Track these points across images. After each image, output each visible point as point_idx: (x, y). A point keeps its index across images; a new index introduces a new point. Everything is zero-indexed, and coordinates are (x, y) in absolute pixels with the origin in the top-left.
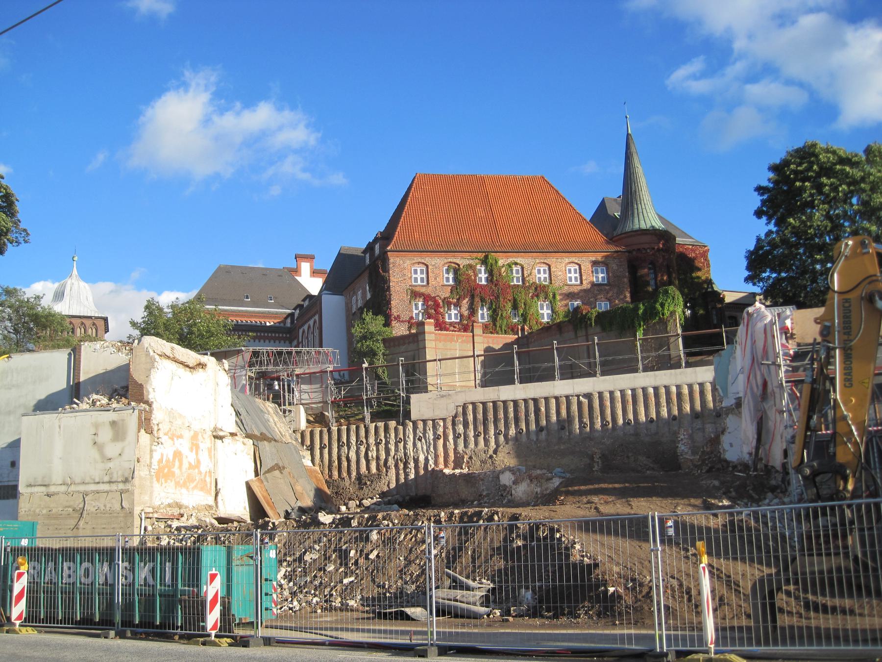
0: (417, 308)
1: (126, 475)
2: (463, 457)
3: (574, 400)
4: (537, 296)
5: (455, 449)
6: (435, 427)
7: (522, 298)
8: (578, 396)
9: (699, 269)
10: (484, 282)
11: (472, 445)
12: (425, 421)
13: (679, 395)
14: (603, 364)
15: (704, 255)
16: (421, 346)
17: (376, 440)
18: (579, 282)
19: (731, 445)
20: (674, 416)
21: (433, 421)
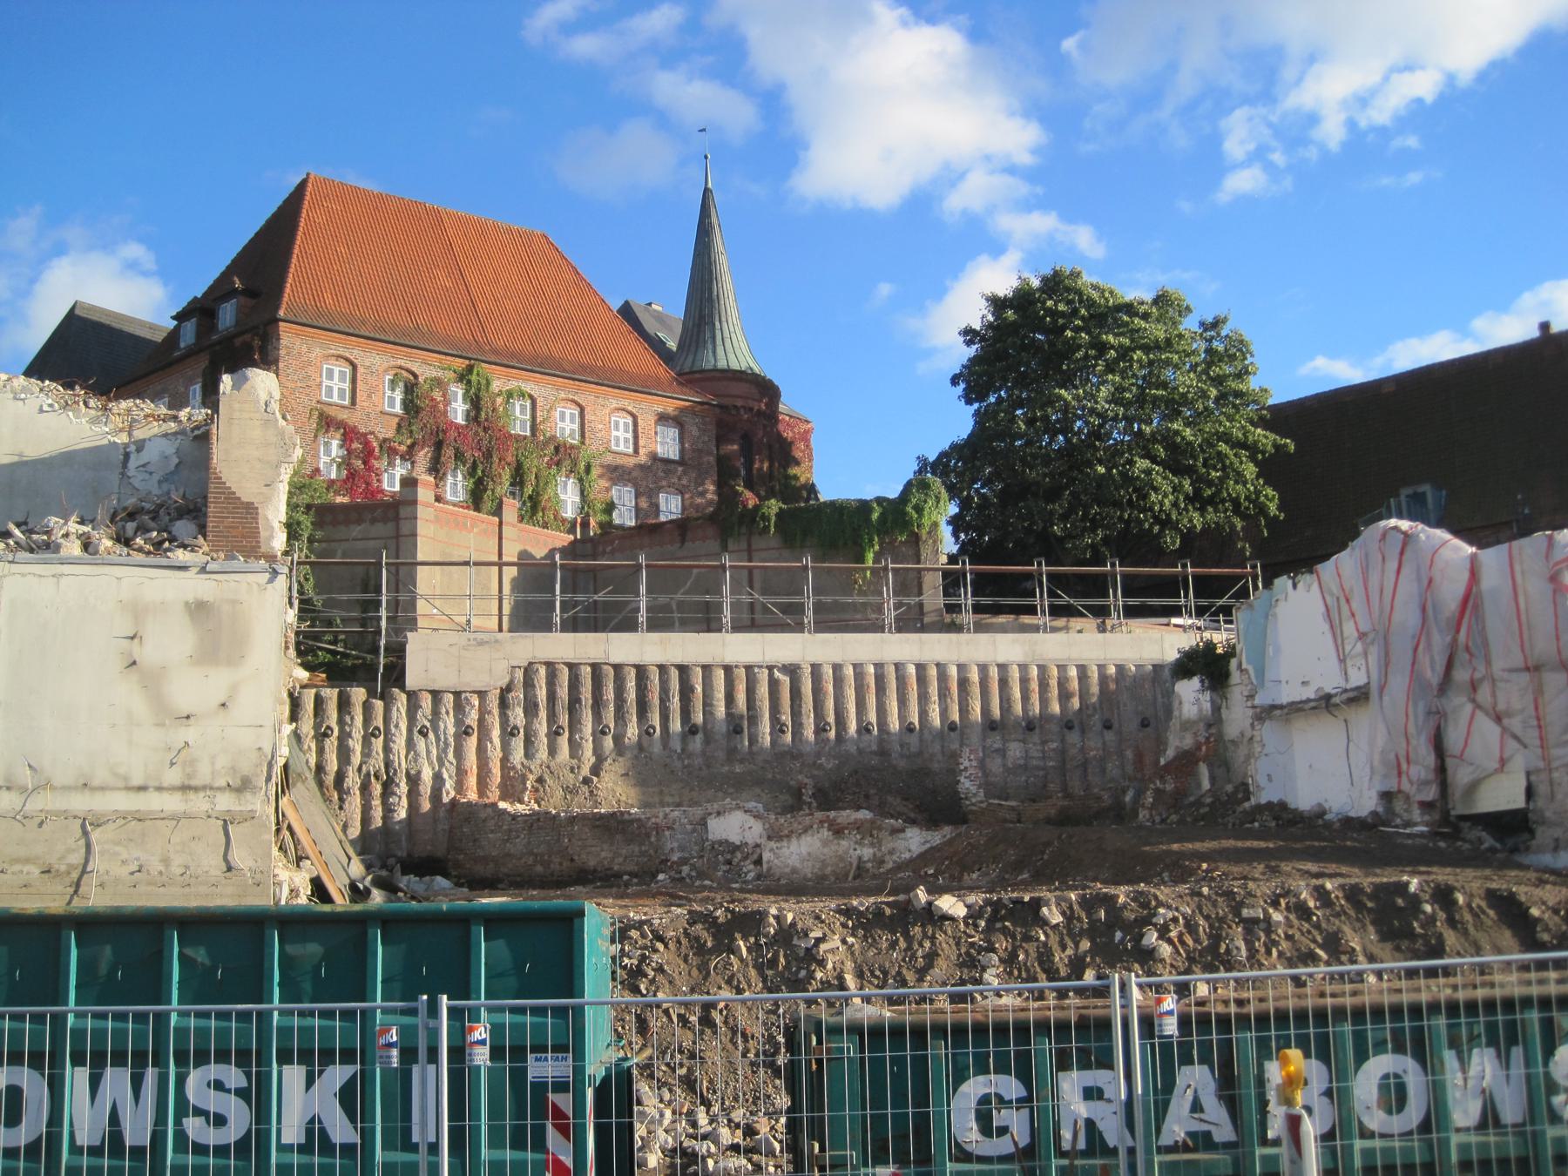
0: (328, 453)
1: (246, 768)
2: (524, 779)
3: (763, 676)
4: (558, 464)
5: (505, 760)
6: (459, 707)
7: (533, 464)
8: (770, 668)
9: (798, 463)
10: (460, 420)
11: (542, 754)
12: (436, 695)
13: (963, 683)
14: (818, 607)
15: (805, 437)
16: (405, 530)
17: (317, 726)
18: (631, 451)
19: (1269, 777)
20: (953, 723)
21: (457, 694)
